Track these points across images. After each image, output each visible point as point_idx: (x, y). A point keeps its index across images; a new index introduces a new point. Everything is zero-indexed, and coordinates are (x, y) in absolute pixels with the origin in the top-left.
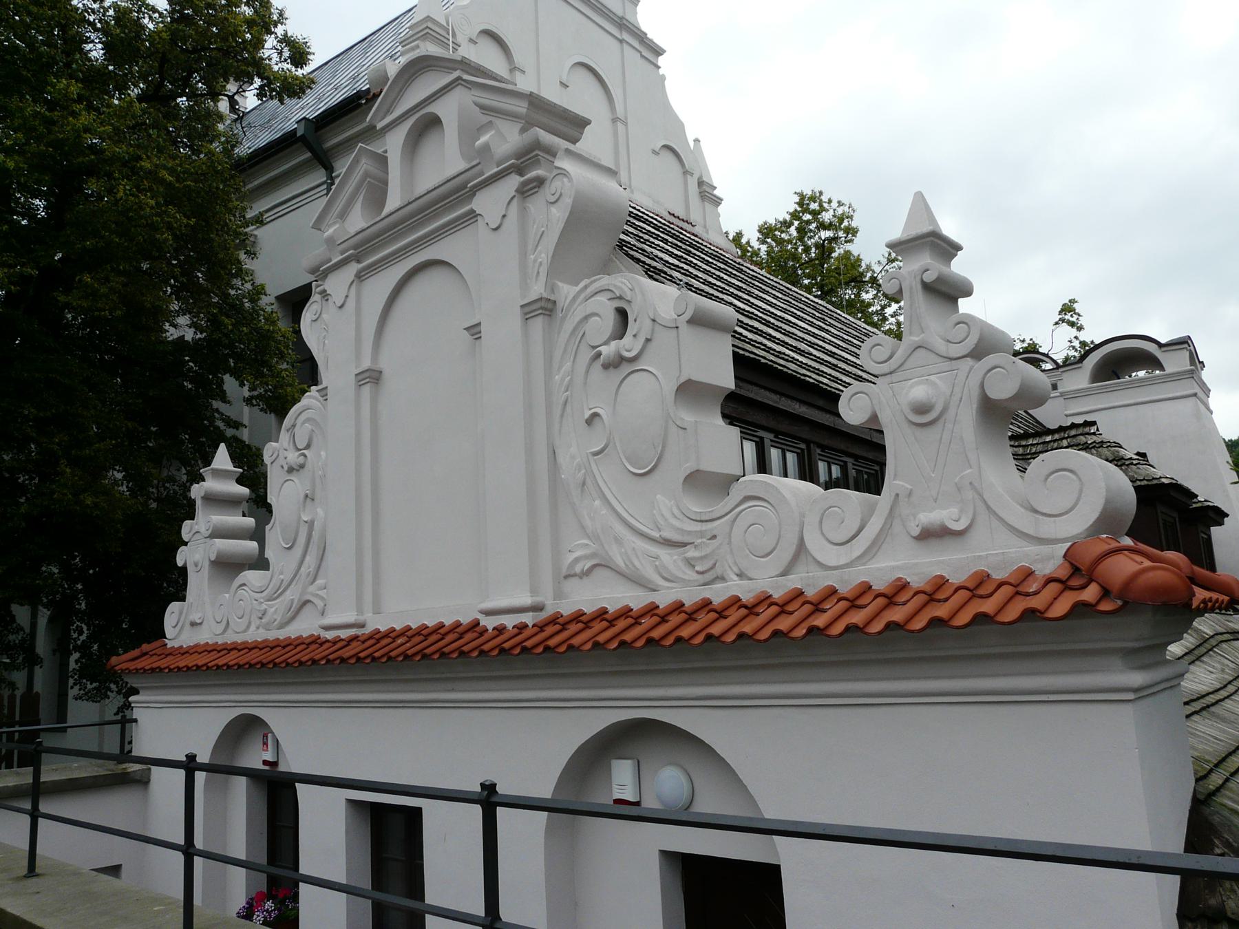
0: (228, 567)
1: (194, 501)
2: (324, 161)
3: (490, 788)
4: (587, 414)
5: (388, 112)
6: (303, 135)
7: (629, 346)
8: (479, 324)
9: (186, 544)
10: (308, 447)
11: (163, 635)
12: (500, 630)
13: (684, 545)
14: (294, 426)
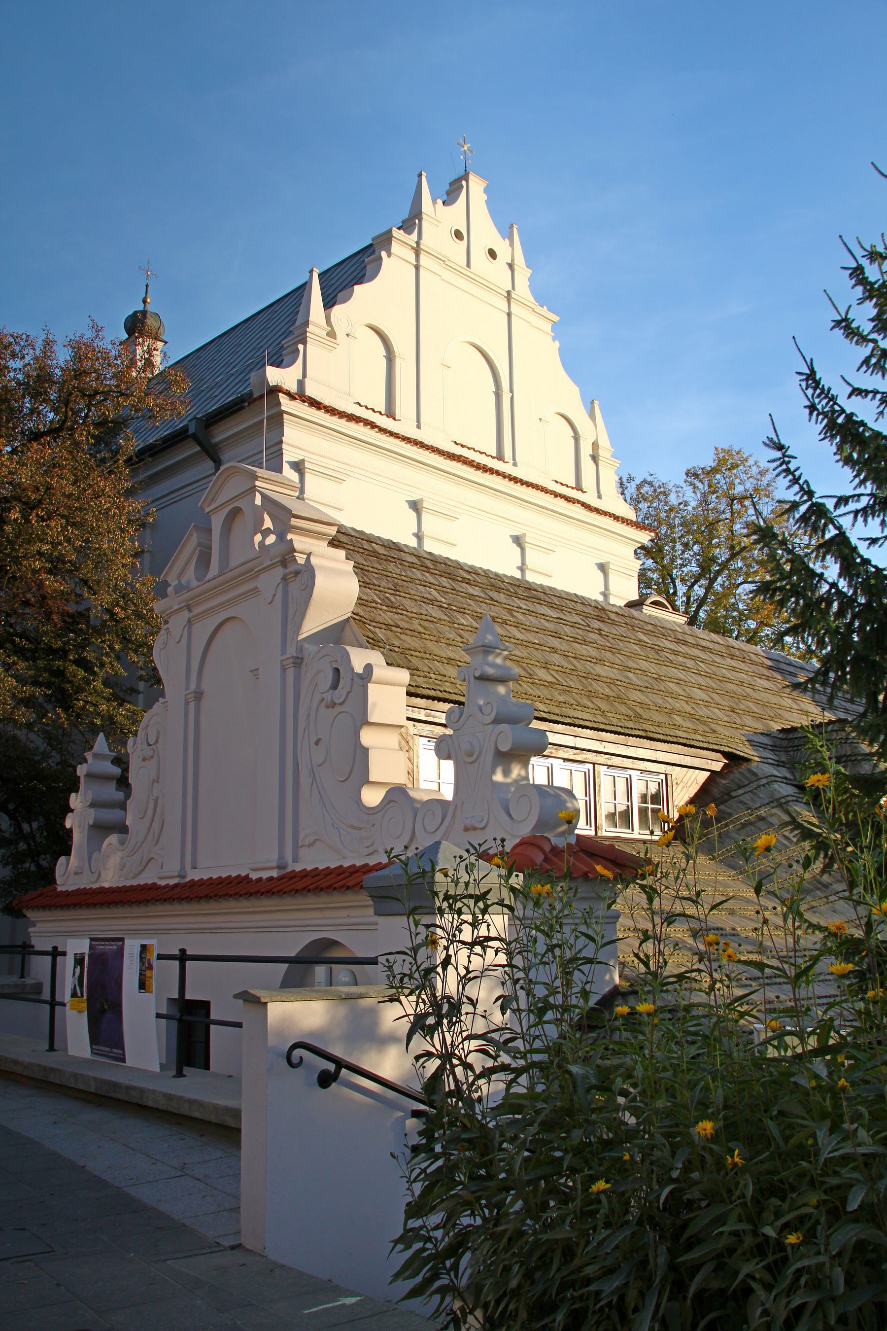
0: (101, 829)
1: (79, 777)
2: (213, 454)
3: (183, 951)
4: (315, 740)
5: (213, 500)
6: (194, 434)
7: (339, 694)
8: (257, 669)
9: (72, 811)
10: (156, 742)
11: (53, 881)
12: (260, 880)
13: (360, 829)
14: (147, 726)
